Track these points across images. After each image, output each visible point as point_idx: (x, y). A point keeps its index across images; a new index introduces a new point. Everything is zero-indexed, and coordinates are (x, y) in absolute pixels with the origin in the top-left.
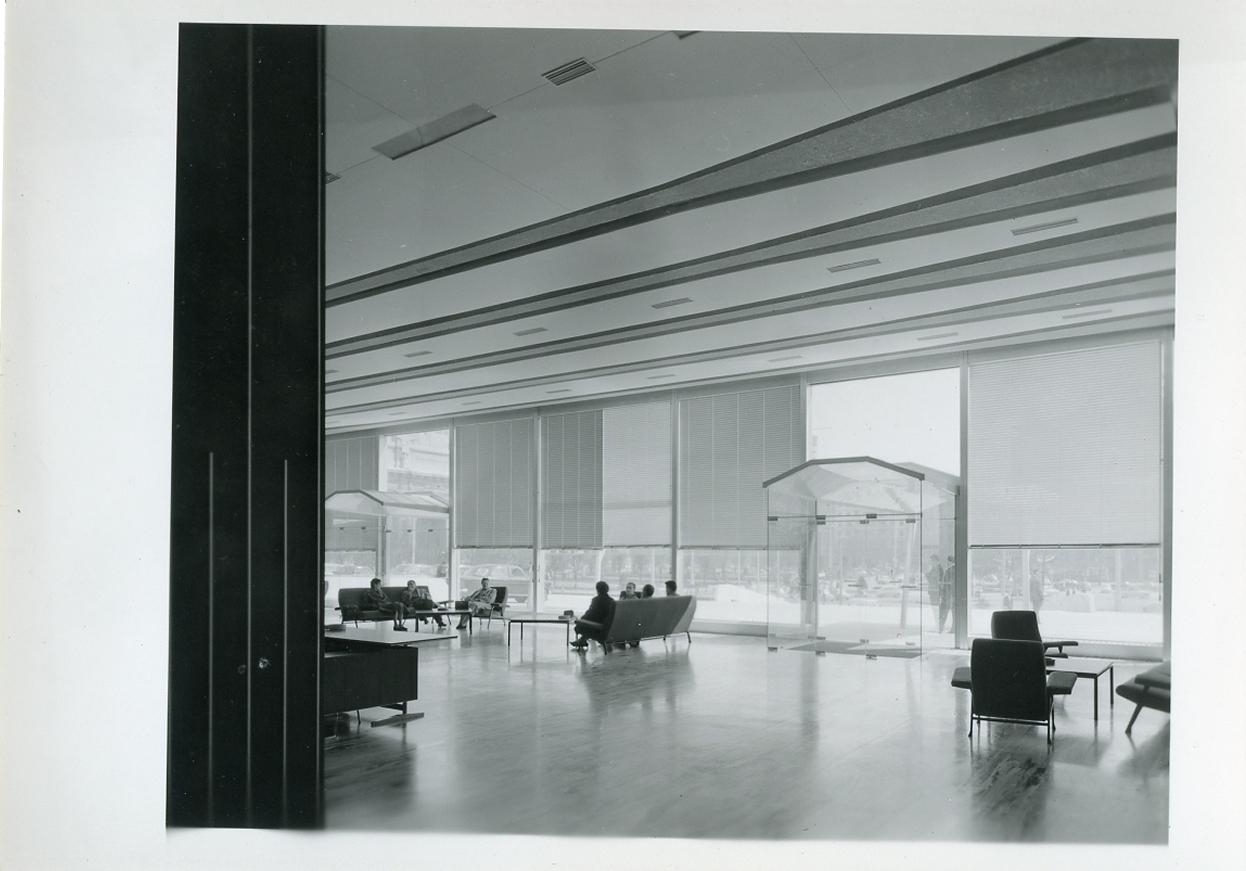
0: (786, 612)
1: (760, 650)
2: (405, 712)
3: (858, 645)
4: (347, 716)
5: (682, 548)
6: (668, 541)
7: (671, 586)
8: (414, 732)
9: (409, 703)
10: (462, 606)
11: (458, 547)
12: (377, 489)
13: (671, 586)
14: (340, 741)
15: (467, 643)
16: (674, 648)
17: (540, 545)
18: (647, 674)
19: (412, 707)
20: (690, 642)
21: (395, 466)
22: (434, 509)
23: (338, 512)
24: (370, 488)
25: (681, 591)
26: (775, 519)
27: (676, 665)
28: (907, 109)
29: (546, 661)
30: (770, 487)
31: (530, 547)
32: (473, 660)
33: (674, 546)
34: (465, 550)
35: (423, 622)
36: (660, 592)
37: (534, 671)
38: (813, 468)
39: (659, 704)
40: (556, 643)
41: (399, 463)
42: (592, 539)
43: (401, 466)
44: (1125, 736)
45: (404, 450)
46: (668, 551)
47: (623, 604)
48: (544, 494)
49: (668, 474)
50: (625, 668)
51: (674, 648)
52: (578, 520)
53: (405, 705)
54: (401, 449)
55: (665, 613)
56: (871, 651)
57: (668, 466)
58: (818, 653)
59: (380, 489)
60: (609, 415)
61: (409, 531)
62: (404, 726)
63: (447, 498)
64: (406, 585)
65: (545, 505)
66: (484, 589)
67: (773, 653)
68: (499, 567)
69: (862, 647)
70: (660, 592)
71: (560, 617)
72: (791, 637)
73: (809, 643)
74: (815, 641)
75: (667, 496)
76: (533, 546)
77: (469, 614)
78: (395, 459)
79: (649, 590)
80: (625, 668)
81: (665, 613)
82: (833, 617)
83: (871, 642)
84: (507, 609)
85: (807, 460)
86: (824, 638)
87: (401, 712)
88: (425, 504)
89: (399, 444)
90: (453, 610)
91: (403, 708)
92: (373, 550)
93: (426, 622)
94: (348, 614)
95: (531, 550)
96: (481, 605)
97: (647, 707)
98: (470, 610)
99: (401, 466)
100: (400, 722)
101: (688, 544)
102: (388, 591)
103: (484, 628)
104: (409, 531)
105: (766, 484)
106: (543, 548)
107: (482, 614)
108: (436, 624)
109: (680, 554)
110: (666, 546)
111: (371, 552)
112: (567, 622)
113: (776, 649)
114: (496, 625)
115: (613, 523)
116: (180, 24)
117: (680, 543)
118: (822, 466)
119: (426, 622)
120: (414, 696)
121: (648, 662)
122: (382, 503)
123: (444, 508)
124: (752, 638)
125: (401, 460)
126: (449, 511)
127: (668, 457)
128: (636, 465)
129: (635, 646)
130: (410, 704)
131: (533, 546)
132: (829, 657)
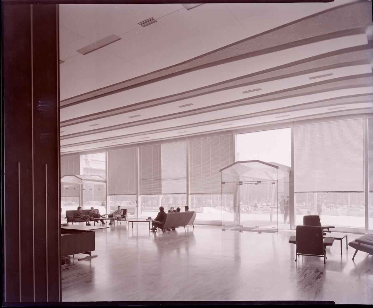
0: (228, 217)
2: (90, 255)
4: (69, 257)
5: (190, 194)
6: (185, 192)
10: (111, 216)
11: (109, 195)
12: (79, 174)
13: (187, 208)
15: (113, 230)
16: (188, 230)
17: (139, 194)
19: (93, 253)
20: (194, 228)
21: (86, 166)
22: (100, 181)
24: (77, 174)
25: (190, 210)
26: (224, 183)
27: (189, 237)
29: (141, 236)
30: (223, 171)
31: (135, 195)
32: (115, 236)
33: (187, 194)
36: (183, 210)
40: (145, 229)
43: (88, 166)
44: (352, 261)
45: (89, 160)
48: (140, 175)
51: (188, 230)
52: (152, 183)
54: (88, 159)
55: (185, 218)
56: (259, 230)
57: (185, 164)
58: (240, 231)
59: (81, 174)
60: (163, 146)
61: (91, 189)
62: (90, 260)
64: (90, 209)
66: (119, 210)
67: (224, 232)
69: (256, 229)
70: (183, 210)
71: (146, 220)
75: (185, 175)
76: (136, 194)
78: (86, 163)
79: (179, 209)
80: (170, 238)
81: (185, 218)
83: (259, 227)
86: (242, 226)
87: (89, 255)
88: (98, 179)
89: (87, 158)
91: (90, 254)
92: (78, 196)
93: (98, 222)
95: (136, 196)
98: (114, 218)
99: (88, 166)
103: (119, 224)
104: (91, 189)
105: (221, 170)
106: (140, 195)
108: (101, 223)
109: (190, 196)
110: (184, 193)
112: (149, 221)
113: (225, 230)
114: (123, 223)
115: (165, 186)
117: (190, 192)
118: (241, 164)
121: (179, 235)
122: (81, 179)
123: (104, 181)
125: (88, 163)
126: (106, 182)
128: (174, 165)
129: (174, 230)
131: (136, 194)
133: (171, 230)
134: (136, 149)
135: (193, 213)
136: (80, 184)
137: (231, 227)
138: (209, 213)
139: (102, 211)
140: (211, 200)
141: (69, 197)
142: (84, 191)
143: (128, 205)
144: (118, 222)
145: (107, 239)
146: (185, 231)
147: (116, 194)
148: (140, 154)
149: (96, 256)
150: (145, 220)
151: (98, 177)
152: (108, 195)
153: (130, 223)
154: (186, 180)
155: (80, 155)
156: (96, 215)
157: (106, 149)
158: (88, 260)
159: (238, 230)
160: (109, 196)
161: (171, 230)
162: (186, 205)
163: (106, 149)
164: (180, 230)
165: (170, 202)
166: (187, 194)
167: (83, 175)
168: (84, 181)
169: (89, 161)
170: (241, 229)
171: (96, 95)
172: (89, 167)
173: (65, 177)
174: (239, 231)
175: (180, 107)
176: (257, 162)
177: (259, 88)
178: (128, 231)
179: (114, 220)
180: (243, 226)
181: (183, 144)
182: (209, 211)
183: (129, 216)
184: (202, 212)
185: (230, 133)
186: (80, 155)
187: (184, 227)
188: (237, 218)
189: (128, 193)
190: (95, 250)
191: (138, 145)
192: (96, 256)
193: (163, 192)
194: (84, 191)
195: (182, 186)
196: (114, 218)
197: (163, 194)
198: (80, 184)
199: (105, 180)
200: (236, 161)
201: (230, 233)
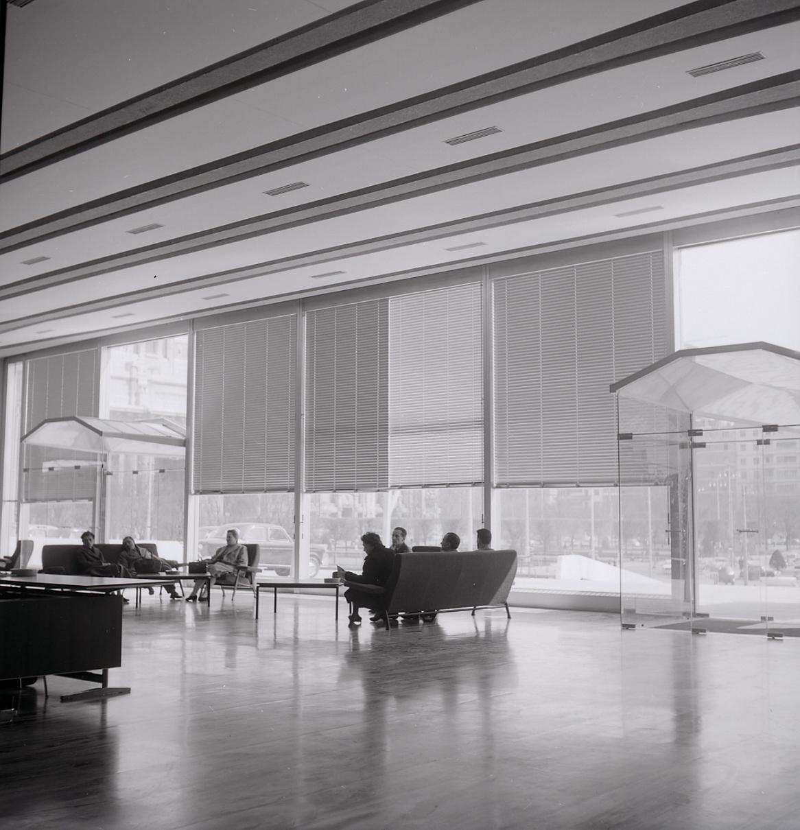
0: (647, 582)
1: (607, 632)
2: (105, 684)
3: (757, 623)
4: (33, 690)
5: (499, 486)
6: (478, 475)
7: (484, 536)
8: (115, 709)
9: (110, 670)
10: (198, 569)
11: (197, 492)
12: (96, 415)
13: (484, 536)
14: (20, 715)
15: (203, 617)
16: (488, 626)
17: (304, 488)
18: (442, 652)
19: (115, 677)
20: (509, 617)
21: (130, 403)
23: (50, 449)
24: (89, 415)
25: (496, 544)
26: (628, 436)
27: (487, 653)
28: (690, 457)
29: (308, 647)
30: (623, 392)
31: (291, 490)
32: (214, 640)
33: (487, 484)
34: (206, 497)
35: (147, 590)
36: (468, 543)
37: (296, 659)
38: (681, 362)
39: (468, 696)
40: (325, 620)
41: (134, 399)
42: (373, 477)
43: (137, 403)
45: (140, 382)
46: (480, 490)
47: (412, 557)
48: (310, 416)
49: (478, 385)
50: (412, 645)
51: (488, 626)
52: (351, 441)
53: (105, 673)
54: (137, 381)
55: (474, 574)
56: (771, 630)
57: (478, 372)
58: (696, 631)
59: (101, 416)
60: (396, 305)
62: (104, 702)
63: (184, 427)
65: (310, 432)
66: (230, 546)
67: (628, 633)
68: (254, 527)
69: (762, 626)
70: (468, 543)
71: (326, 580)
72: (658, 615)
73: (684, 620)
74: (692, 619)
75: (476, 413)
76: (295, 489)
77: (207, 578)
78: (130, 394)
79: (452, 540)
80: (412, 645)
81: (474, 574)
82: (712, 596)
83: (775, 621)
84: (258, 574)
85: (676, 350)
86: (707, 615)
87: (100, 685)
88: (158, 434)
89: (134, 375)
90: (187, 574)
91: (103, 679)
92: (90, 499)
93: (151, 592)
94: (47, 569)
95: (292, 495)
96: (220, 568)
97: (451, 703)
98: (208, 574)
99: (137, 403)
100: (102, 696)
101: (508, 480)
102: (105, 548)
103: (228, 600)
105: (614, 388)
106: (308, 491)
107: (225, 581)
108: (166, 596)
109: (496, 494)
110: (475, 484)
111: (86, 502)
112: (336, 586)
113: (633, 626)
114: (243, 598)
115: (401, 453)
116: (120, 666)
117: (495, 480)
118: (699, 359)
119: (151, 592)
120: (117, 663)
121: (447, 639)
122: (100, 433)
123: (180, 440)
124: (600, 614)
125: (137, 394)
126: (185, 443)
127: (477, 359)
128: (432, 368)
129: (431, 619)
130: (112, 671)
131: (295, 489)
132: (713, 638)
133: (421, 622)
134: (295, 320)
135: (507, 560)
136: (99, 452)
137: (657, 617)
138: (582, 579)
139: (168, 551)
140: (594, 538)
141: (58, 500)
142: (109, 477)
143: (268, 540)
144: (224, 596)
145: (184, 656)
146: (477, 631)
147: (221, 488)
148: (310, 337)
149: (125, 691)
150: (323, 582)
151: (159, 427)
152: (193, 492)
153: (266, 596)
154: (477, 436)
155: (102, 348)
156: (145, 563)
157: (191, 323)
158: (97, 701)
159: (689, 630)
160: (198, 497)
161: (421, 622)
162: (482, 527)
163: (191, 323)
164: (454, 624)
165: (418, 509)
166: (487, 484)
167: (108, 418)
168: (111, 443)
169: (140, 387)
170: (700, 625)
171: (151, 112)
172: (139, 409)
173: (46, 424)
174: (690, 632)
175: (453, 142)
176: (761, 351)
177: (754, 51)
178: (257, 622)
179: (208, 581)
180: (711, 617)
181: (469, 294)
182: (574, 551)
183: (264, 574)
184: (554, 577)
185: (654, 242)
186: (102, 348)
187: (473, 614)
188: (690, 594)
189: (265, 486)
190: (120, 666)
191: (305, 302)
192: (125, 691)
193: (390, 483)
194: (109, 477)
195: (465, 453)
196: (208, 574)
197: (393, 487)
198: (96, 454)
199: (184, 438)
200: (677, 349)
201: (654, 642)
